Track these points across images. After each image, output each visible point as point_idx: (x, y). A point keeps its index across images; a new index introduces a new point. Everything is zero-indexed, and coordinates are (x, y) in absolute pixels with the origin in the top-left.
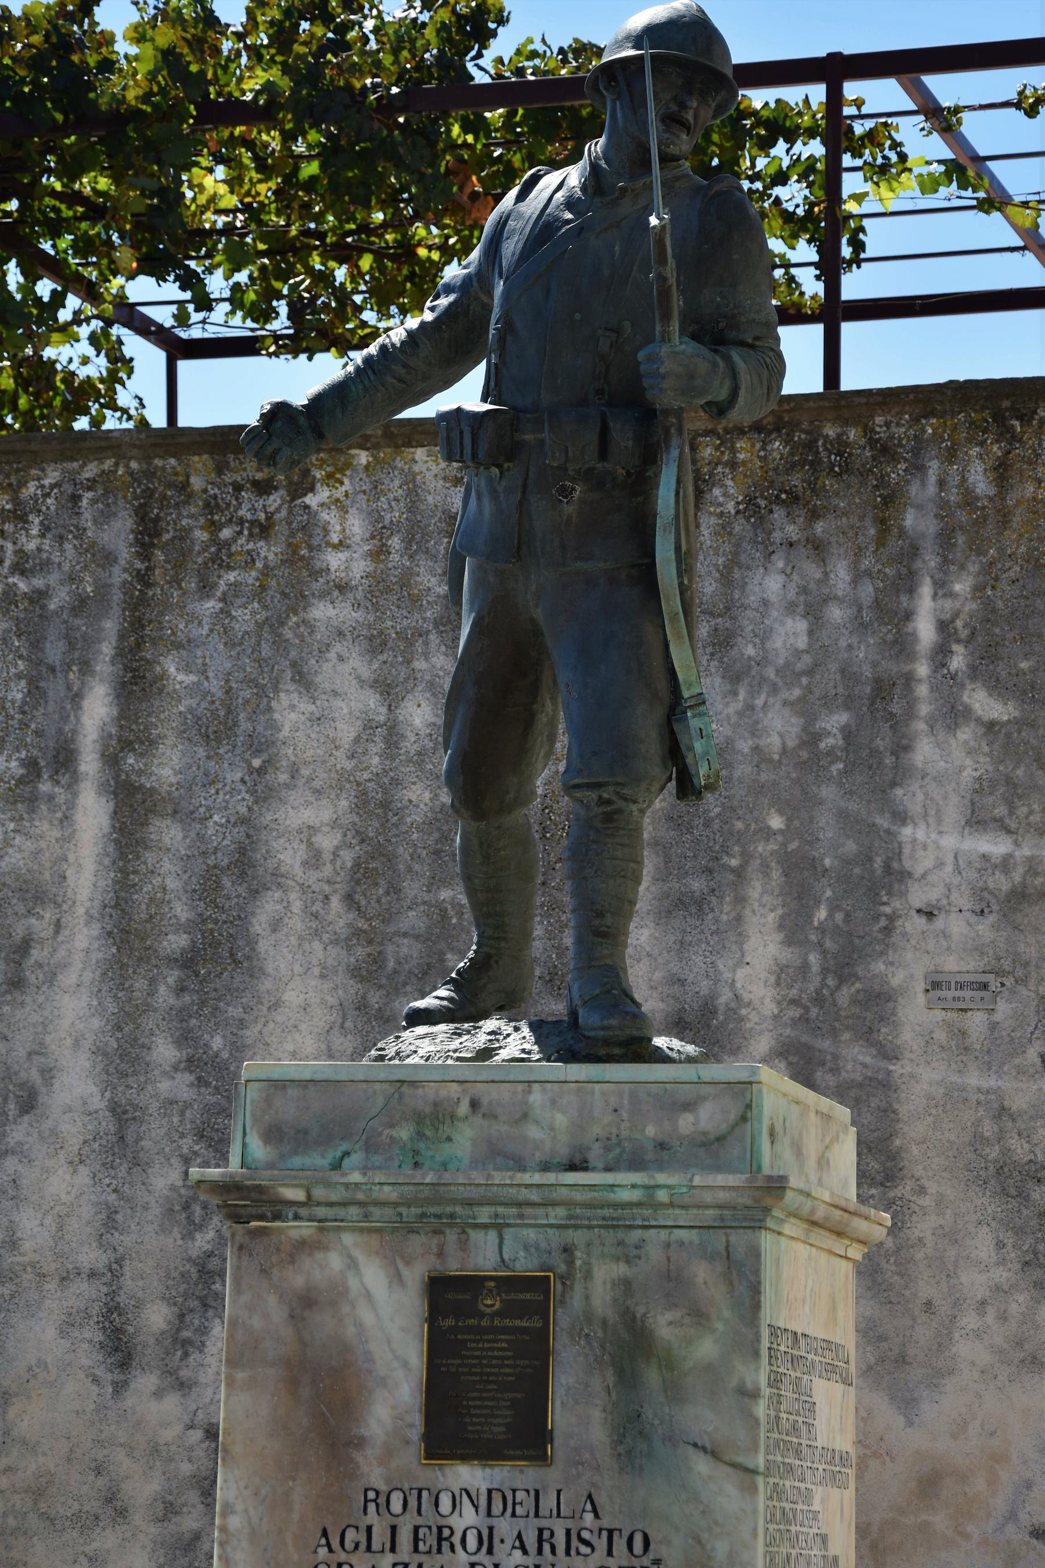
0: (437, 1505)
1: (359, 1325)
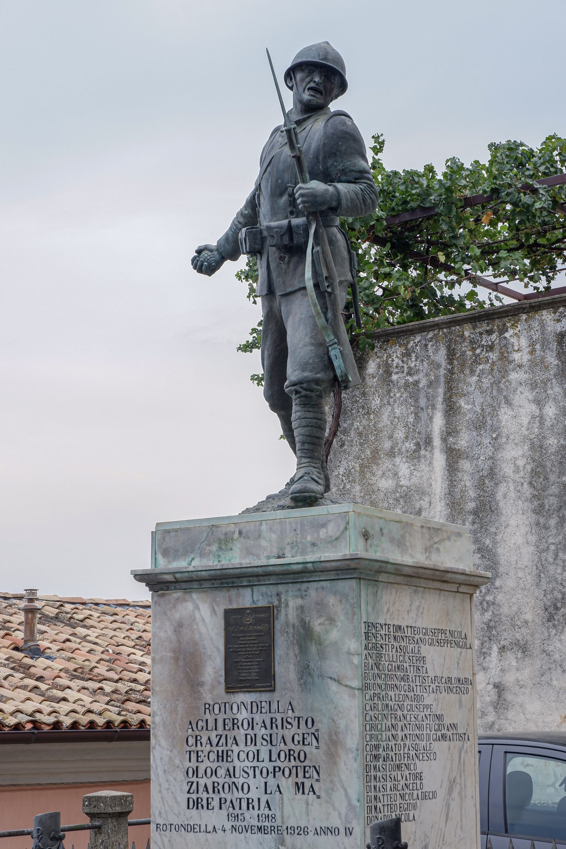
0: (232, 709)
1: (200, 633)
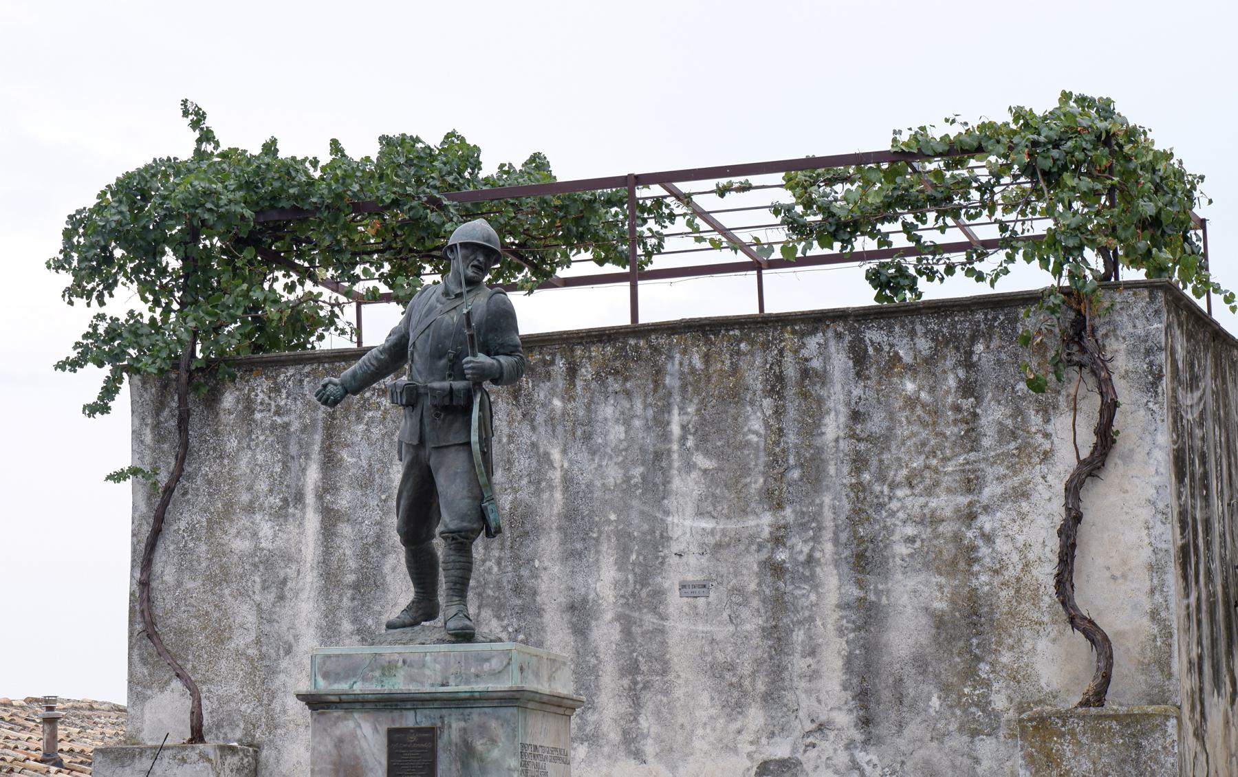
1: (361, 748)
